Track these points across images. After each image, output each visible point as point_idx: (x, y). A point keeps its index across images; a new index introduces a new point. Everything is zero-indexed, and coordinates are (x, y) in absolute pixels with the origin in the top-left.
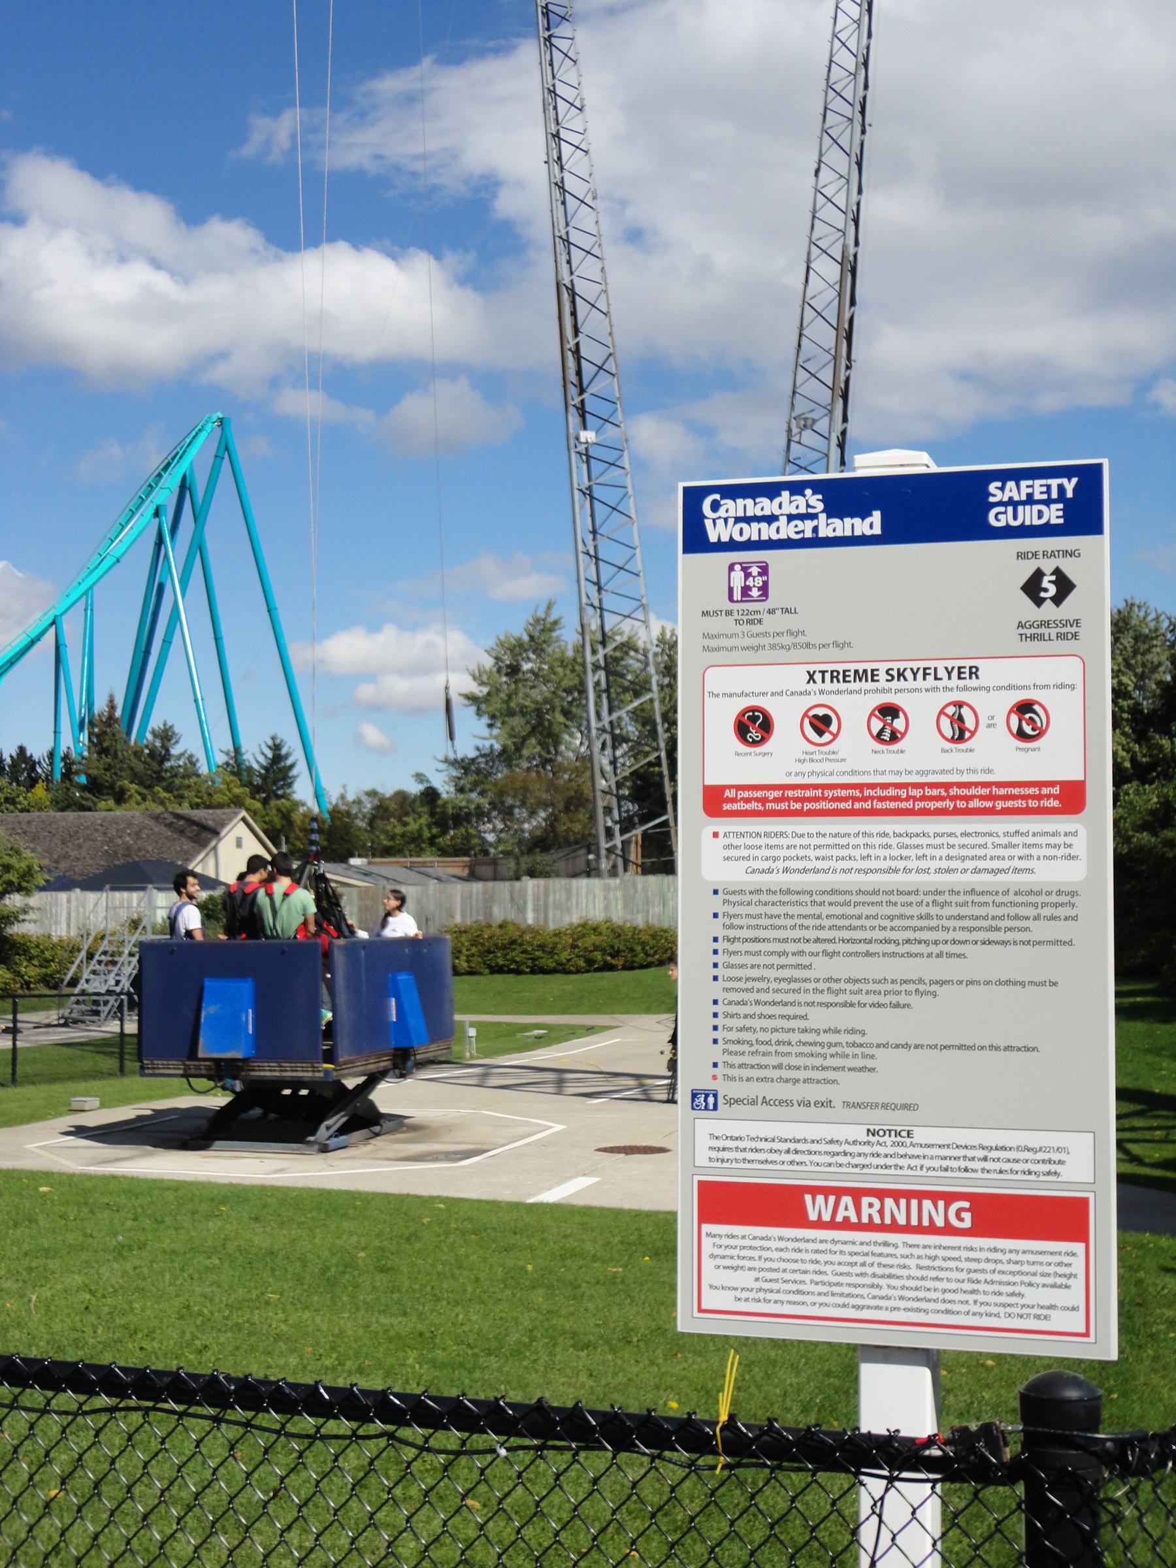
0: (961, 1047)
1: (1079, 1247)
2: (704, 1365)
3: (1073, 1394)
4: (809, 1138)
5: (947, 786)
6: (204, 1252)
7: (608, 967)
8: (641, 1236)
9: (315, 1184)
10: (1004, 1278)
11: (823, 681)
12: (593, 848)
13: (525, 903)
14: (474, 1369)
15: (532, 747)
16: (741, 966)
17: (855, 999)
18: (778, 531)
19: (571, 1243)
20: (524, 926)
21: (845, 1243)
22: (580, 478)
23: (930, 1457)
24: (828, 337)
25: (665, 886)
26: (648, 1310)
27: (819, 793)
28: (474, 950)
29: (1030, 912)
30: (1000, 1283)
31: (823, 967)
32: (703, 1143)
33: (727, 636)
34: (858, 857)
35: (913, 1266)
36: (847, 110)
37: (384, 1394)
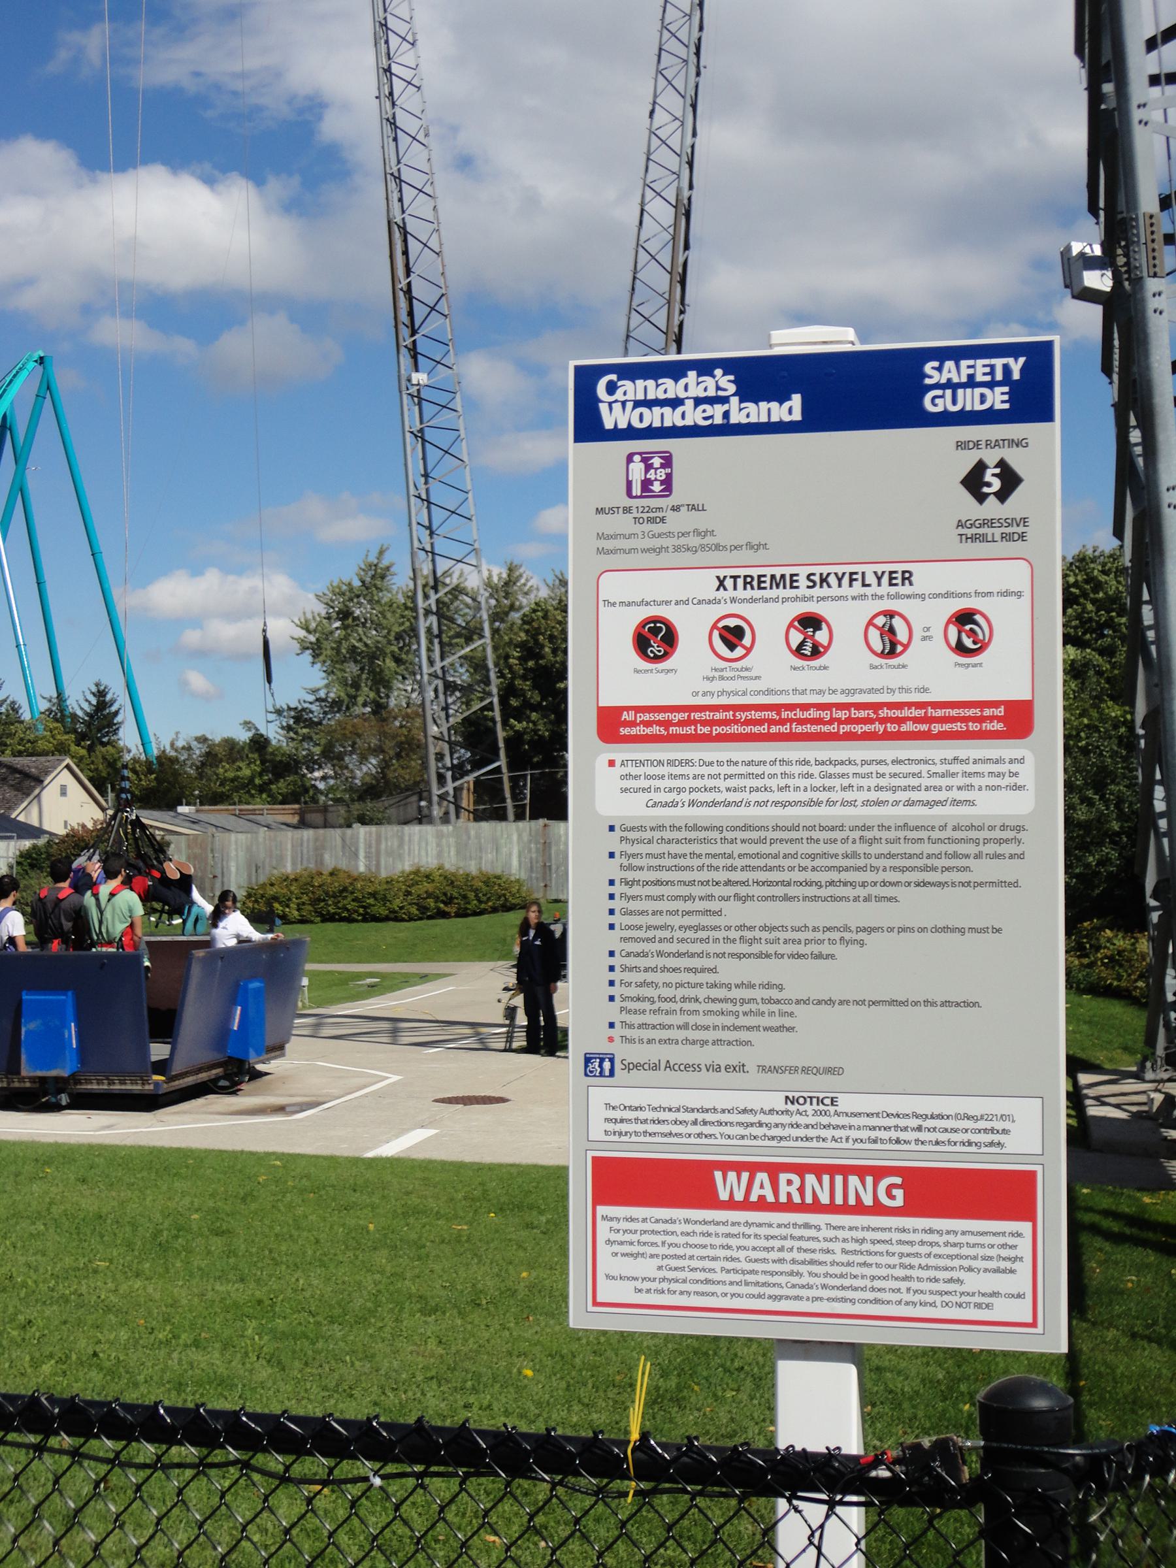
0: (893, 1002)
1: (1025, 1227)
2: (557, 1328)
3: (1040, 1403)
4: (719, 1107)
5: (876, 706)
6: (28, 1217)
7: (443, 915)
8: (485, 1191)
9: (144, 1142)
10: (941, 1262)
11: (735, 588)
12: (425, 794)
13: (357, 850)
14: (317, 1338)
15: (366, 693)
16: (642, 913)
17: (771, 949)
18: (683, 416)
19: (414, 1200)
20: (355, 874)
21: (760, 1225)
22: (412, 420)
23: (877, 1479)
24: (661, 281)
25: (499, 833)
26: (496, 1270)
27: (730, 715)
28: (305, 898)
29: (971, 849)
30: (937, 1268)
31: (735, 913)
32: (598, 1114)
33: (624, 536)
34: (775, 788)
35: (838, 1250)
36: (682, 52)
37: (236, 1414)
